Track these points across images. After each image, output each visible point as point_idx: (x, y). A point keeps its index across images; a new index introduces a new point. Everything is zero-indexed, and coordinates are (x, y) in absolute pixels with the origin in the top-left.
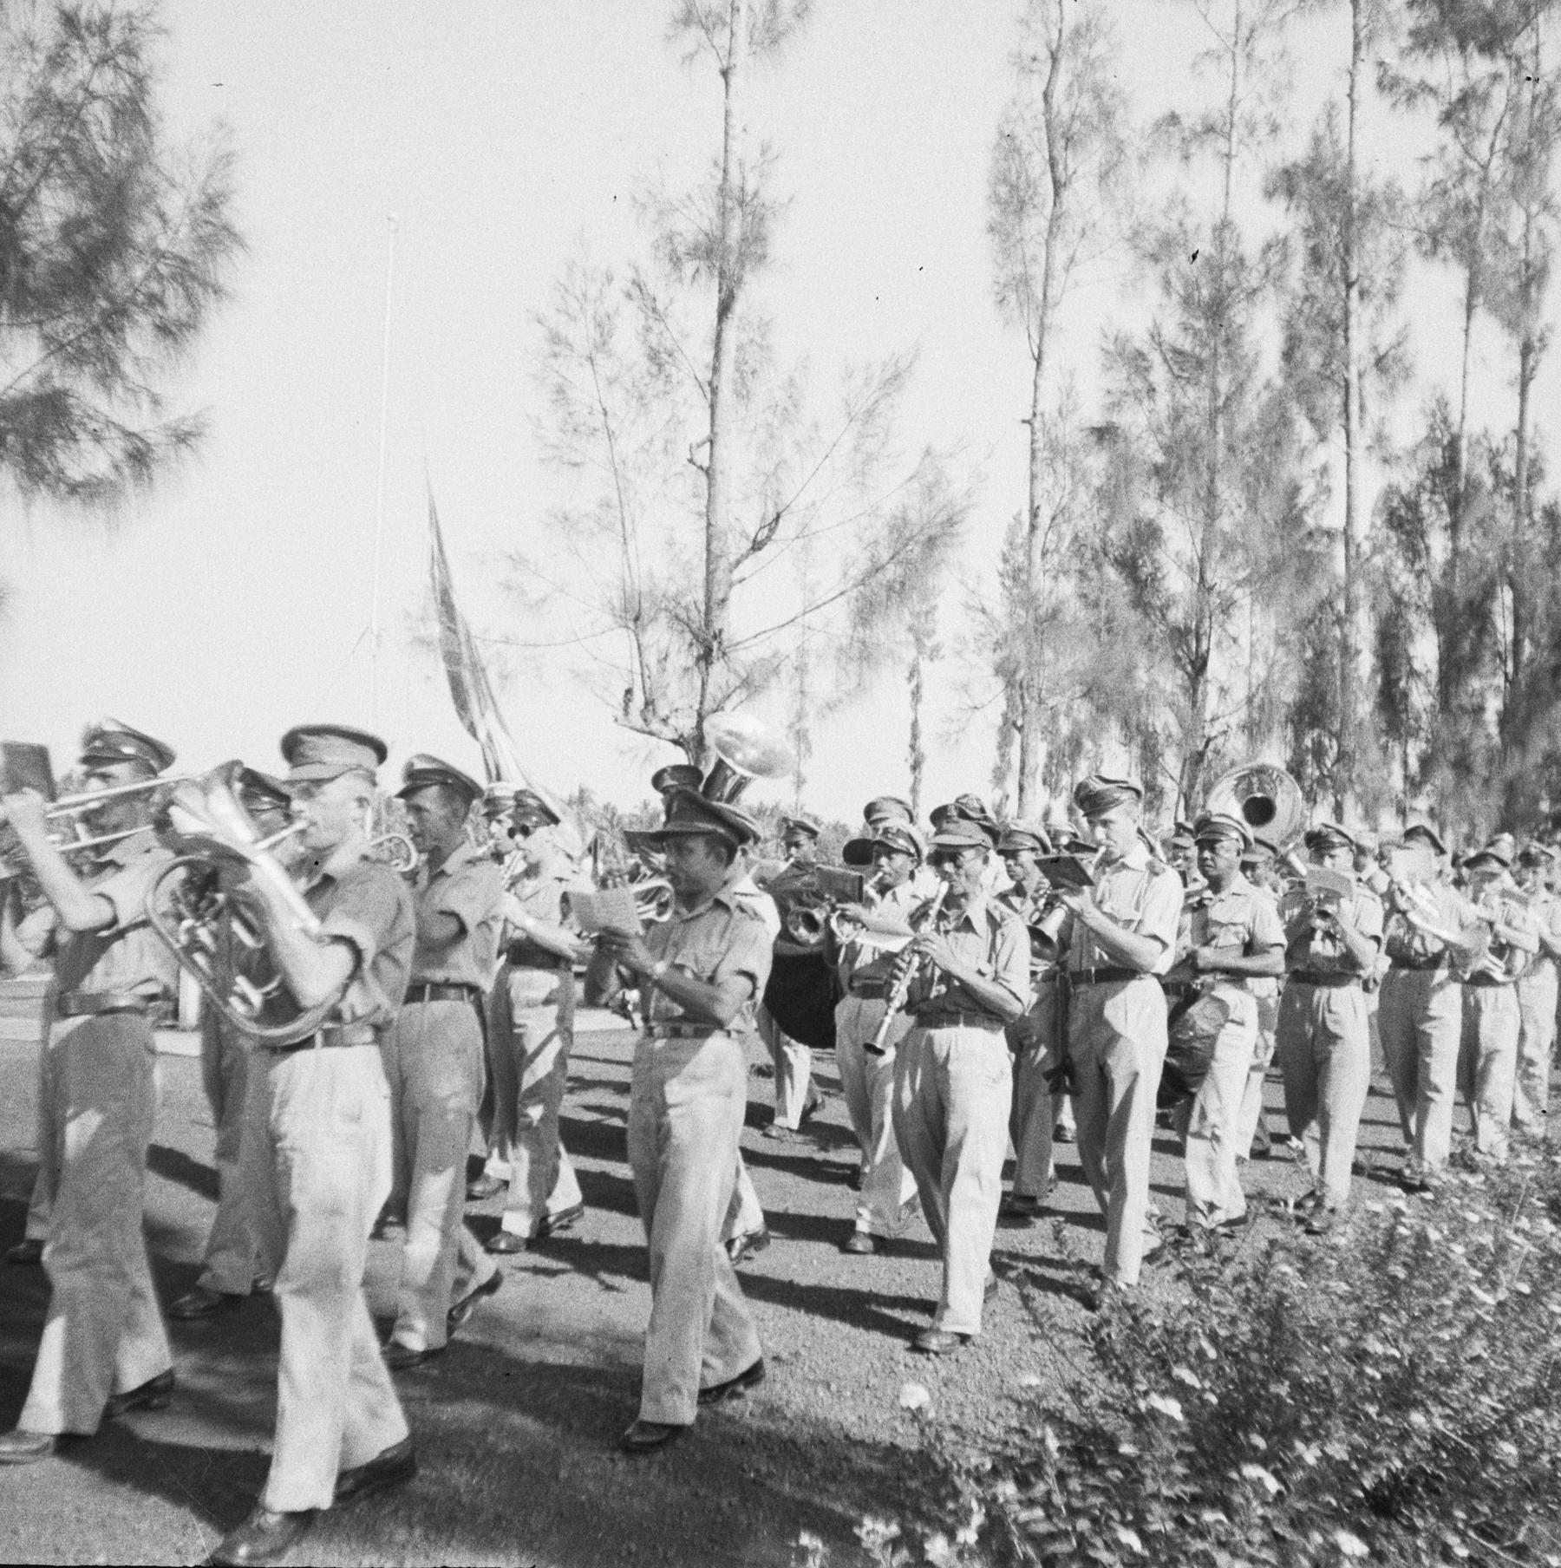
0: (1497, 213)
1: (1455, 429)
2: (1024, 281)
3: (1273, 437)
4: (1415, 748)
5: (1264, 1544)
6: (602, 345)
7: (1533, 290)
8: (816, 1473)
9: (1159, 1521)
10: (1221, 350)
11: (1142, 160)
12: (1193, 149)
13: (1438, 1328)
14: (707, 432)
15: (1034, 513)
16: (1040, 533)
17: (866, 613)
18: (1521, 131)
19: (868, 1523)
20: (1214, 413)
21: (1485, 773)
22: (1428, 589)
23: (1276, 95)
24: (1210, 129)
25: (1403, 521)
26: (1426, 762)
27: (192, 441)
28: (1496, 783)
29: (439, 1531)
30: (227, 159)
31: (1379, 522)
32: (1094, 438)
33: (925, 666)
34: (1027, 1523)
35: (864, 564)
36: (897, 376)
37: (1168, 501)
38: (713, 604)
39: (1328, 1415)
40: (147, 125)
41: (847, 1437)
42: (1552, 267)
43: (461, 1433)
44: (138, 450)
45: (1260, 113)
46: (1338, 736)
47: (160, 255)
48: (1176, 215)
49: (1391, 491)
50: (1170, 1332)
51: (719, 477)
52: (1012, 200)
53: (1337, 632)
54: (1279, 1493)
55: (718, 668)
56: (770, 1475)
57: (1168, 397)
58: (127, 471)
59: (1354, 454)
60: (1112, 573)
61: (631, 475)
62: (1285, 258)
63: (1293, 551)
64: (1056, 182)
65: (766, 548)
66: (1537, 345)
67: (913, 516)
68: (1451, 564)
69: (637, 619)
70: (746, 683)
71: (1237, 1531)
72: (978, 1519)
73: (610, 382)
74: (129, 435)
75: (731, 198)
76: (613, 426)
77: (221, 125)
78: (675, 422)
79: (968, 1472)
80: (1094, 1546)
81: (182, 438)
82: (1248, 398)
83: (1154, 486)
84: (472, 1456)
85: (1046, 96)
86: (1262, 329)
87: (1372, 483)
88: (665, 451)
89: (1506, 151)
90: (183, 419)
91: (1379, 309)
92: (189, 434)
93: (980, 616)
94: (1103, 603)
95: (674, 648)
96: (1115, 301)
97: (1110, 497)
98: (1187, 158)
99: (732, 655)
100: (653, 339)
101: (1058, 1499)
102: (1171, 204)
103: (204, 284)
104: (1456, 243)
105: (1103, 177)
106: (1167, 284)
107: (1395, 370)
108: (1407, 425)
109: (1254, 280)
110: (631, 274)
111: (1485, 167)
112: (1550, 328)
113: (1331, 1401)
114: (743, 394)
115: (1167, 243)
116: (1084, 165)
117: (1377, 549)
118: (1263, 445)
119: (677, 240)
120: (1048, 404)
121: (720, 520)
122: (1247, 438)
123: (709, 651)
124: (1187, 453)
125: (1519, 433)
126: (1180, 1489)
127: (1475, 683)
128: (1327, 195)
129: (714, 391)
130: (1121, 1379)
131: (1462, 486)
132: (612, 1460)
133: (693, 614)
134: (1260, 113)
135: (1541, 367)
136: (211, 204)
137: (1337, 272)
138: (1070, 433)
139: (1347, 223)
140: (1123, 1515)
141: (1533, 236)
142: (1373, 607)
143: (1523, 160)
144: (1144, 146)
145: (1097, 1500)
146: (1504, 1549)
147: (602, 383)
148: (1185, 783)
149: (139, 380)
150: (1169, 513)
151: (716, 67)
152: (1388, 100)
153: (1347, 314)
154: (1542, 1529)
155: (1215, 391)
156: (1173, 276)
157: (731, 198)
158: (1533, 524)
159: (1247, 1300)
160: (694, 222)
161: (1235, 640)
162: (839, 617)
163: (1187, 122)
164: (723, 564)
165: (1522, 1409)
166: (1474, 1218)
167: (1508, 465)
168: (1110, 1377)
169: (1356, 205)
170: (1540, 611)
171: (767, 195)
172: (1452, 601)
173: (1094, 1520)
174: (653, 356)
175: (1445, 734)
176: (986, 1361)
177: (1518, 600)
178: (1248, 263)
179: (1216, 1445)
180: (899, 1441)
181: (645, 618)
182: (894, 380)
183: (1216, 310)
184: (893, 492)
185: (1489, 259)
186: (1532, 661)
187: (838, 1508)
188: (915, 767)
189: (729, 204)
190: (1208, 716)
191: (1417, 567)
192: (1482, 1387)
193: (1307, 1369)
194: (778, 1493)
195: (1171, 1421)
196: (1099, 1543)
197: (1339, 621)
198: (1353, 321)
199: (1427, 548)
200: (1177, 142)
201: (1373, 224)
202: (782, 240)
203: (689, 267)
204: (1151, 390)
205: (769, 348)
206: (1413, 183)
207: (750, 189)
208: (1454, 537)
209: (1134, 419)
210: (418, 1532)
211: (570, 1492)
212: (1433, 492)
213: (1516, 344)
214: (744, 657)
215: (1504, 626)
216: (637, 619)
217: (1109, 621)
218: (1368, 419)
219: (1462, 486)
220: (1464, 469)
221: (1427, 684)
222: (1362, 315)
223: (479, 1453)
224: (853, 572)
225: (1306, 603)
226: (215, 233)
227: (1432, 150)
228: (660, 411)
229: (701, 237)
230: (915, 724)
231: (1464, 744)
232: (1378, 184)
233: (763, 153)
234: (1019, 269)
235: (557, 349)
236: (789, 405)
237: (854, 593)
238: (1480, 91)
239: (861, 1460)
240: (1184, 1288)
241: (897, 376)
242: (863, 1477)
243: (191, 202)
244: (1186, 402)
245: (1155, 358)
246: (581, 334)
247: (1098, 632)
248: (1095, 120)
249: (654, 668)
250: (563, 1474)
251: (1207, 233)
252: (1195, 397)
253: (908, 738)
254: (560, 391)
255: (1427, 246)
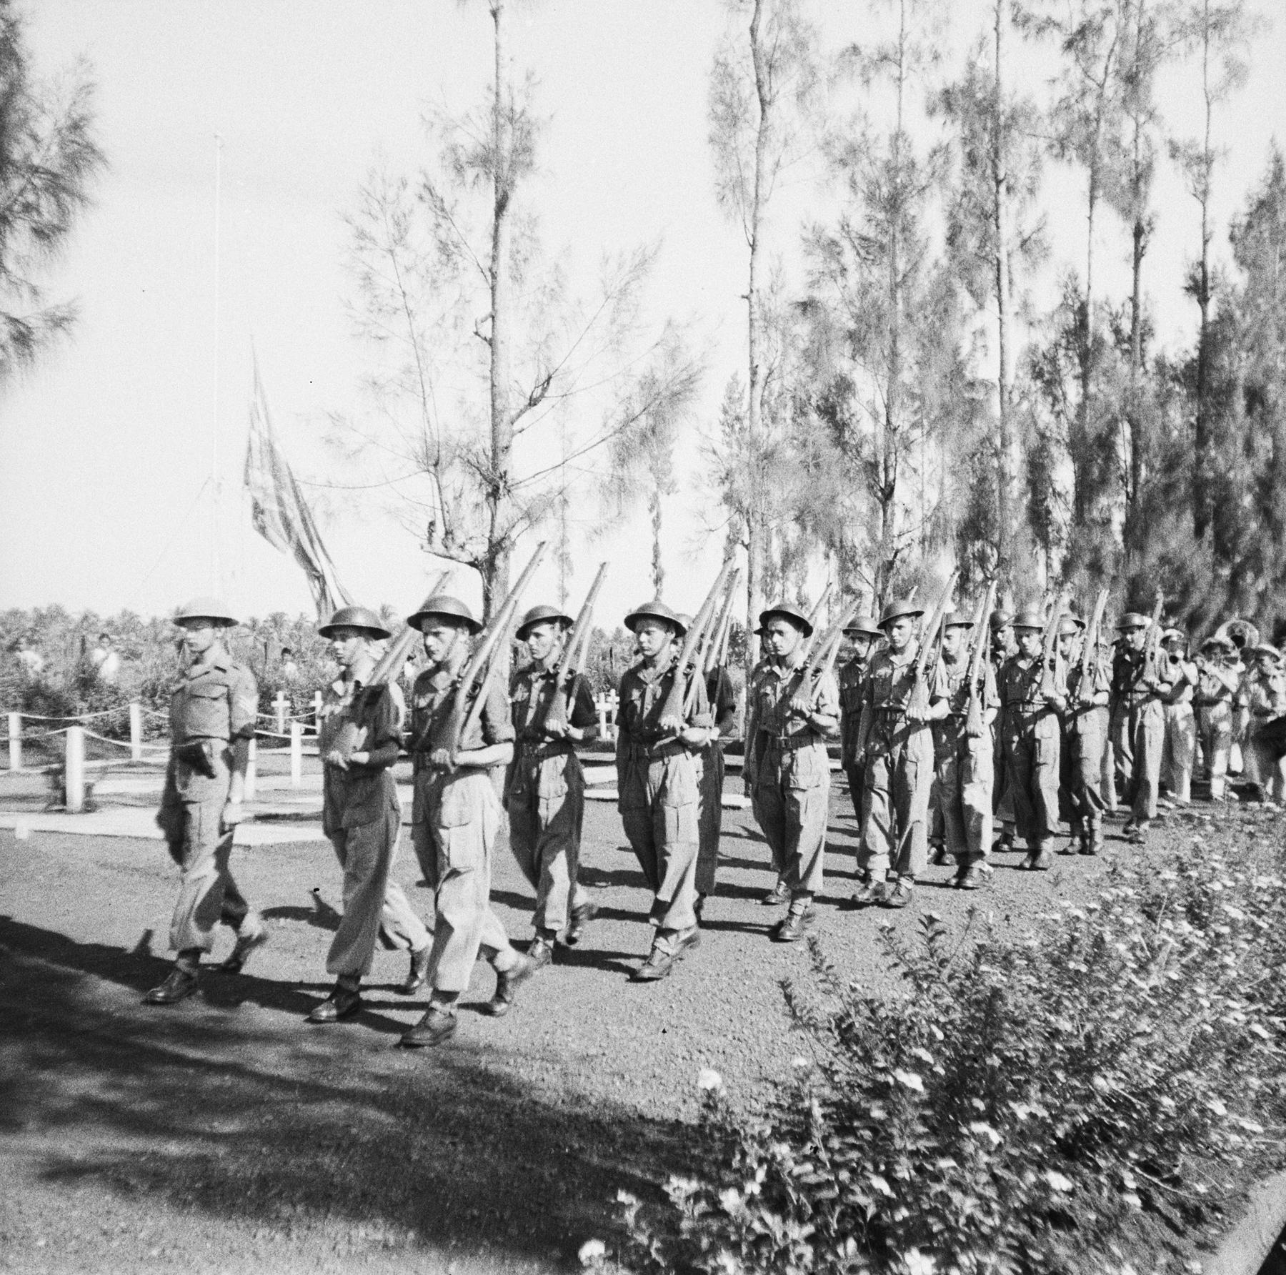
0: (1111, 123)
1: (1083, 298)
2: (740, 183)
3: (941, 307)
4: (1058, 554)
5: (988, 1183)
6: (400, 240)
7: (1141, 185)
8: (618, 1146)
9: (904, 1171)
10: (899, 236)
11: (832, 81)
12: (872, 74)
13: (1111, 1008)
14: (490, 309)
15: (754, 372)
16: (758, 388)
17: (623, 457)
18: (1130, 55)
19: (675, 1180)
20: (894, 287)
21: (1112, 572)
22: (1065, 427)
23: (937, 29)
24: (885, 58)
25: (1046, 375)
26: (1068, 566)
27: (65, 324)
28: (1123, 582)
29: (317, 1207)
30: (87, 89)
31: (1021, 374)
32: (799, 311)
33: (663, 498)
34: (799, 1176)
35: (621, 416)
36: (644, 262)
37: (860, 359)
38: (498, 451)
39: (1027, 1082)
40: (19, 62)
41: (641, 1117)
42: (1155, 165)
43: (330, 1127)
44: (21, 333)
45: (925, 44)
46: (997, 546)
47: (35, 170)
48: (858, 129)
49: (1033, 350)
50: (898, 1022)
51: (500, 346)
52: (728, 116)
53: (995, 463)
54: (1000, 1145)
55: (504, 502)
56: (581, 1150)
57: (857, 276)
58: (11, 350)
59: (1005, 318)
60: (814, 417)
61: (428, 346)
62: (947, 162)
63: (959, 401)
64: (762, 101)
65: (540, 405)
66: (1146, 228)
67: (659, 375)
68: (1081, 408)
69: (436, 465)
70: (528, 515)
71: (968, 1175)
72: (761, 1175)
73: (408, 270)
74: (14, 321)
75: (503, 116)
76: (411, 305)
77: (82, 61)
78: (464, 301)
79: (753, 1137)
80: (853, 1192)
81: (58, 322)
82: (921, 274)
83: (848, 348)
84: (339, 1145)
85: (753, 31)
86: (930, 219)
87: (1019, 340)
88: (455, 326)
89: (1117, 72)
90: (58, 307)
91: (1023, 201)
92: (64, 319)
93: (714, 458)
94: (809, 444)
95: (467, 487)
96: (813, 201)
97: (813, 357)
98: (867, 82)
99: (514, 492)
100: (442, 233)
101: (823, 1155)
102: (855, 119)
103: (71, 193)
104: (1080, 147)
105: (800, 96)
106: (853, 184)
107: (1036, 251)
108: (1046, 296)
109: (922, 179)
110: (422, 180)
111: (1101, 86)
112: (1155, 214)
113: (1030, 1070)
114: (517, 278)
115: (853, 150)
116: (784, 86)
117: (1024, 396)
118: (934, 313)
119: (460, 151)
120: (762, 283)
121: (502, 381)
122: (922, 307)
123: (496, 490)
124: (873, 321)
125: (1134, 300)
126: (922, 1145)
127: (1103, 501)
128: (981, 113)
129: (494, 276)
130: (861, 1060)
131: (1089, 343)
132: (454, 1144)
133: (483, 459)
134: (925, 44)
135: (1149, 247)
136: (76, 127)
137: (989, 172)
138: (780, 305)
139: (996, 133)
140: (876, 1167)
141: (1141, 140)
142: (1024, 443)
143: (1131, 79)
144: (833, 70)
145: (854, 1155)
146: (1163, 1181)
147: (401, 270)
148: (880, 586)
149: (20, 274)
150: (860, 370)
151: (487, 8)
152: (1021, 33)
153: (997, 205)
154: (1192, 1164)
155: (895, 271)
156: (859, 178)
157: (503, 116)
158: (1146, 372)
159: (961, 993)
160: (474, 136)
161: (915, 471)
162: (603, 459)
163: (865, 52)
164: (506, 418)
165: (1175, 1070)
166: (1128, 921)
167: (1126, 326)
168: (851, 1059)
169: (1002, 118)
170: (1154, 442)
171: (532, 114)
172: (1084, 437)
173: (852, 1171)
174: (444, 248)
175: (1082, 543)
176: (747, 1052)
177: (1136, 433)
178: (918, 166)
179: (949, 1105)
180: (682, 1118)
181: (443, 462)
182: (642, 265)
183: (893, 204)
184: (643, 358)
185: (1106, 160)
186: (1147, 482)
187: (638, 1173)
188: (658, 581)
189: (502, 121)
190: (895, 532)
191: (1057, 408)
192: (1148, 1053)
193: (1013, 1046)
194: (588, 1164)
195: (914, 1092)
196: (857, 1189)
197: (996, 454)
198: (1002, 211)
199: (1064, 394)
200: (858, 68)
201: (1015, 133)
202: (544, 152)
203: (470, 173)
204: (844, 270)
205: (537, 241)
206: (1044, 101)
207: (518, 109)
208: (1085, 386)
209: (830, 295)
210: (300, 1209)
211: (421, 1171)
212: (1067, 349)
213: (1130, 227)
214: (524, 494)
215: (1124, 454)
216: (436, 465)
217: (815, 457)
218: (1015, 292)
219: (1089, 343)
220: (1091, 329)
221: (1066, 503)
222: (1009, 206)
223: (345, 1144)
224: (611, 422)
225: (971, 439)
226: (79, 151)
227: (1056, 73)
228: (450, 293)
229: (479, 149)
230: (656, 545)
231: (1096, 550)
232: (1018, 100)
233: (528, 78)
234: (735, 173)
235: (362, 243)
236: (555, 286)
237: (613, 439)
238: (1095, 24)
239: (652, 1134)
240: (909, 984)
241: (644, 262)
242: (655, 1147)
243: (59, 125)
244: (872, 279)
245: (845, 244)
246: (381, 230)
247: (807, 467)
248: (793, 50)
249: (452, 504)
250: (415, 1157)
251: (885, 141)
252: (879, 275)
253: (651, 559)
254: (367, 278)
255: (1056, 150)
